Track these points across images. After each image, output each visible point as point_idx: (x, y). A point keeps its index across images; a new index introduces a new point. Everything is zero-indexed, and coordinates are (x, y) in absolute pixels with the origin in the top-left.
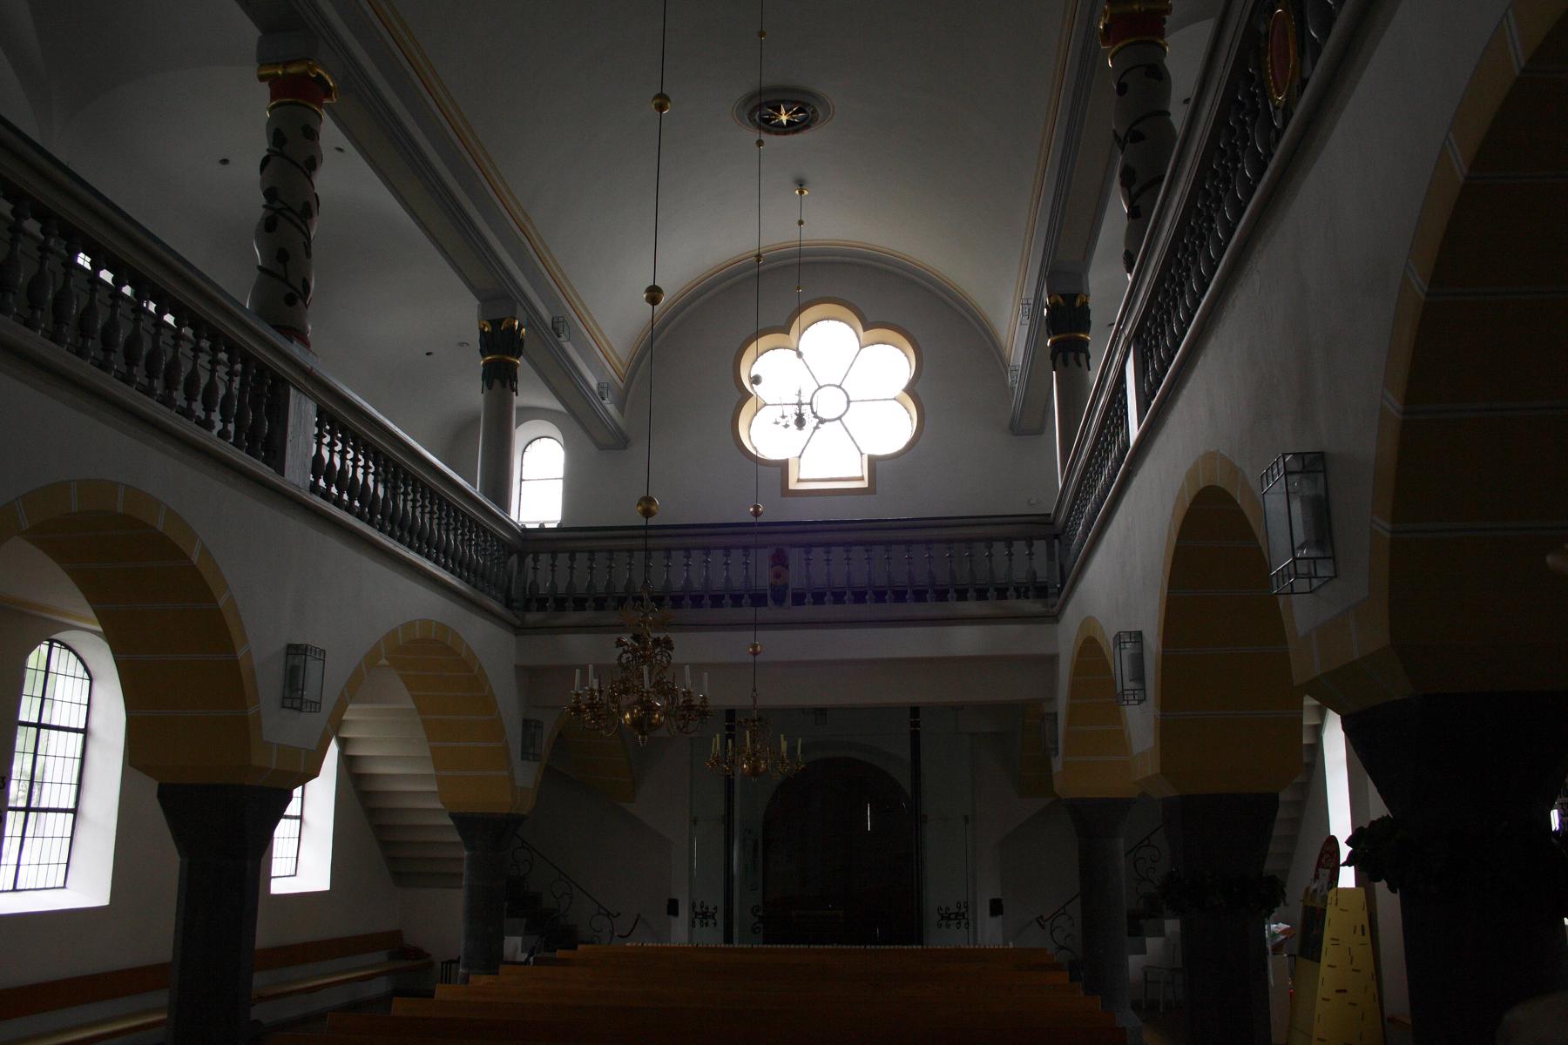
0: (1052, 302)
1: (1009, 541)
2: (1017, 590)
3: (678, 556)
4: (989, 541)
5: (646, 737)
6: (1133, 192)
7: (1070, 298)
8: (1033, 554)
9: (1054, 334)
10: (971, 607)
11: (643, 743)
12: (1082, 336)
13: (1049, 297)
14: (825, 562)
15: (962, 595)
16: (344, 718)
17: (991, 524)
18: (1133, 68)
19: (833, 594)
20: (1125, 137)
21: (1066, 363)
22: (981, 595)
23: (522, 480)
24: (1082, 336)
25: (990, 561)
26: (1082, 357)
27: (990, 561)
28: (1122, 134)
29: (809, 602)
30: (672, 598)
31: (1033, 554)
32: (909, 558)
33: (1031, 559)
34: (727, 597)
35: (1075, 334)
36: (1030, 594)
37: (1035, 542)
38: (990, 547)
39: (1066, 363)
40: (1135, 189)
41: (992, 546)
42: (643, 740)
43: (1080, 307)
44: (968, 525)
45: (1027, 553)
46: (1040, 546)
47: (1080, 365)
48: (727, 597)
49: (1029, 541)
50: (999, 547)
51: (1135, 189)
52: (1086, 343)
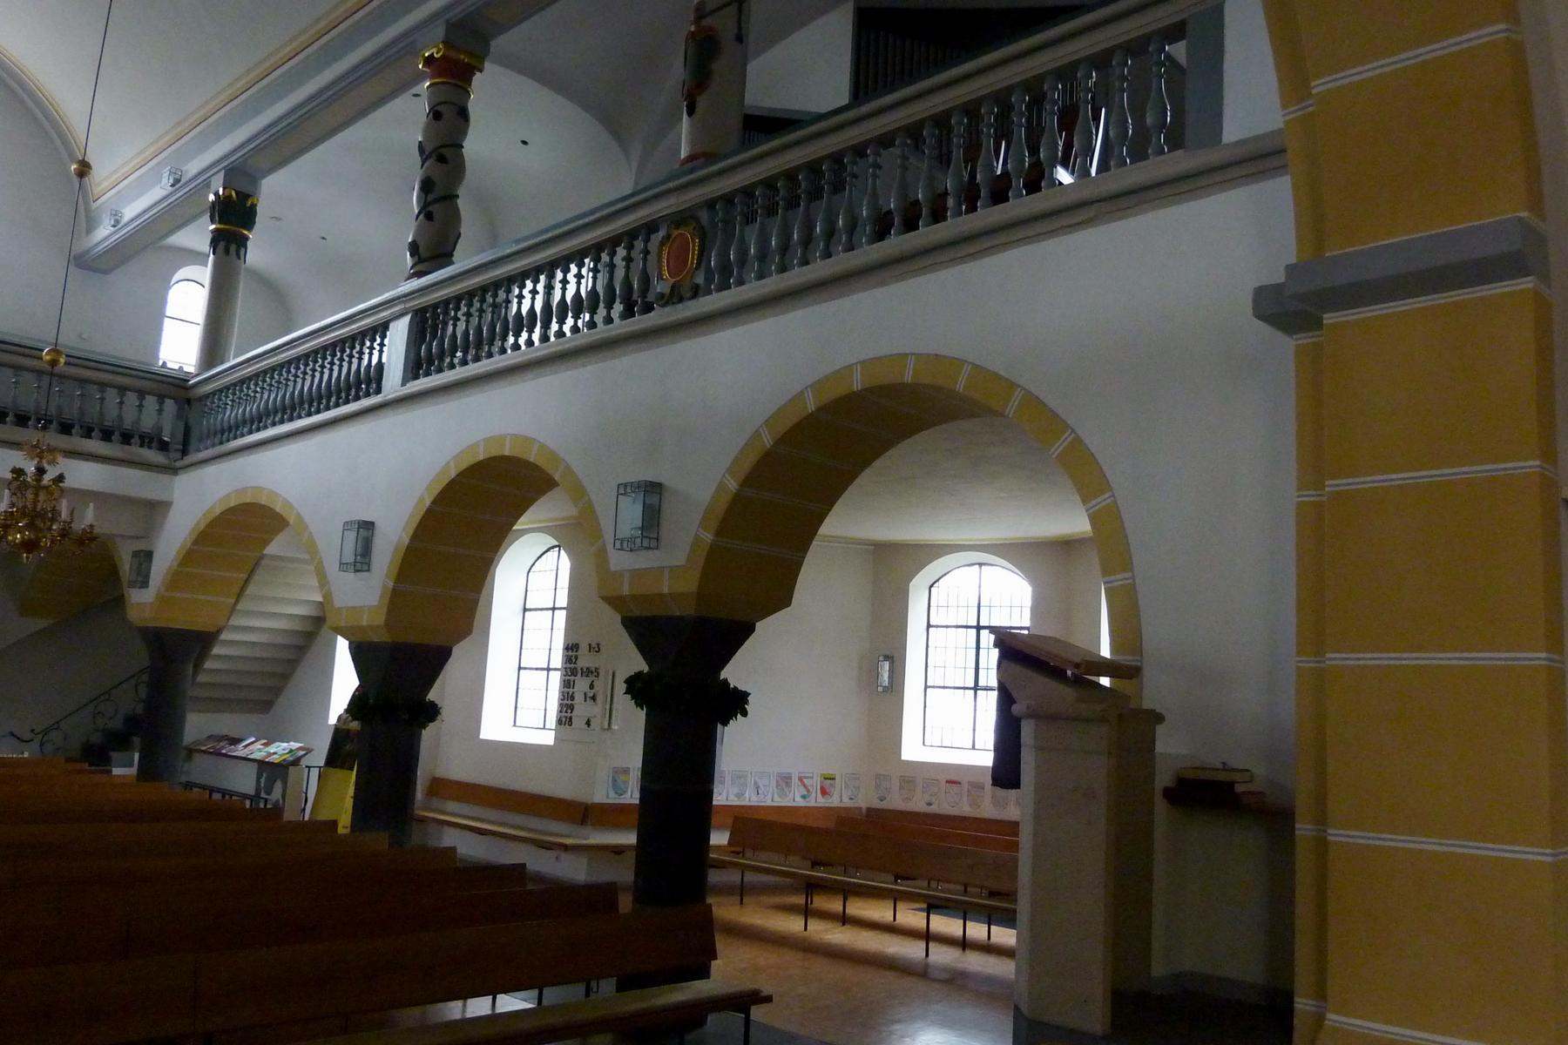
0: (226, 194)
1: (142, 394)
2: (142, 437)
3: (112, 396)
4: (123, 390)
5: (31, 556)
6: (429, 199)
7: (244, 196)
8: (143, 407)
9: (220, 223)
10: (94, 445)
11: (27, 560)
12: (246, 232)
13: (224, 189)
14: (137, 409)
15: (88, 433)
16: (272, 549)
17: (150, 380)
18: (445, 103)
19: (16, 416)
20: (431, 153)
21: (227, 252)
22: (107, 435)
23: (981, 565)
24: (246, 232)
25: (102, 403)
26: (243, 251)
27: (102, 403)
28: (428, 150)
29: (136, 444)
30: (142, 437)
31: (143, 407)
32: (38, 387)
33: (141, 410)
34: (117, 434)
35: (241, 230)
36: (153, 445)
37: (147, 396)
38: (103, 392)
39: (227, 252)
40: (431, 197)
41: (164, 402)
42: (27, 558)
43: (249, 208)
44: (113, 372)
45: (137, 404)
46: (170, 405)
47: (239, 258)
48: (117, 434)
49: (161, 398)
50: (132, 398)
51: (431, 197)
52: (247, 238)
